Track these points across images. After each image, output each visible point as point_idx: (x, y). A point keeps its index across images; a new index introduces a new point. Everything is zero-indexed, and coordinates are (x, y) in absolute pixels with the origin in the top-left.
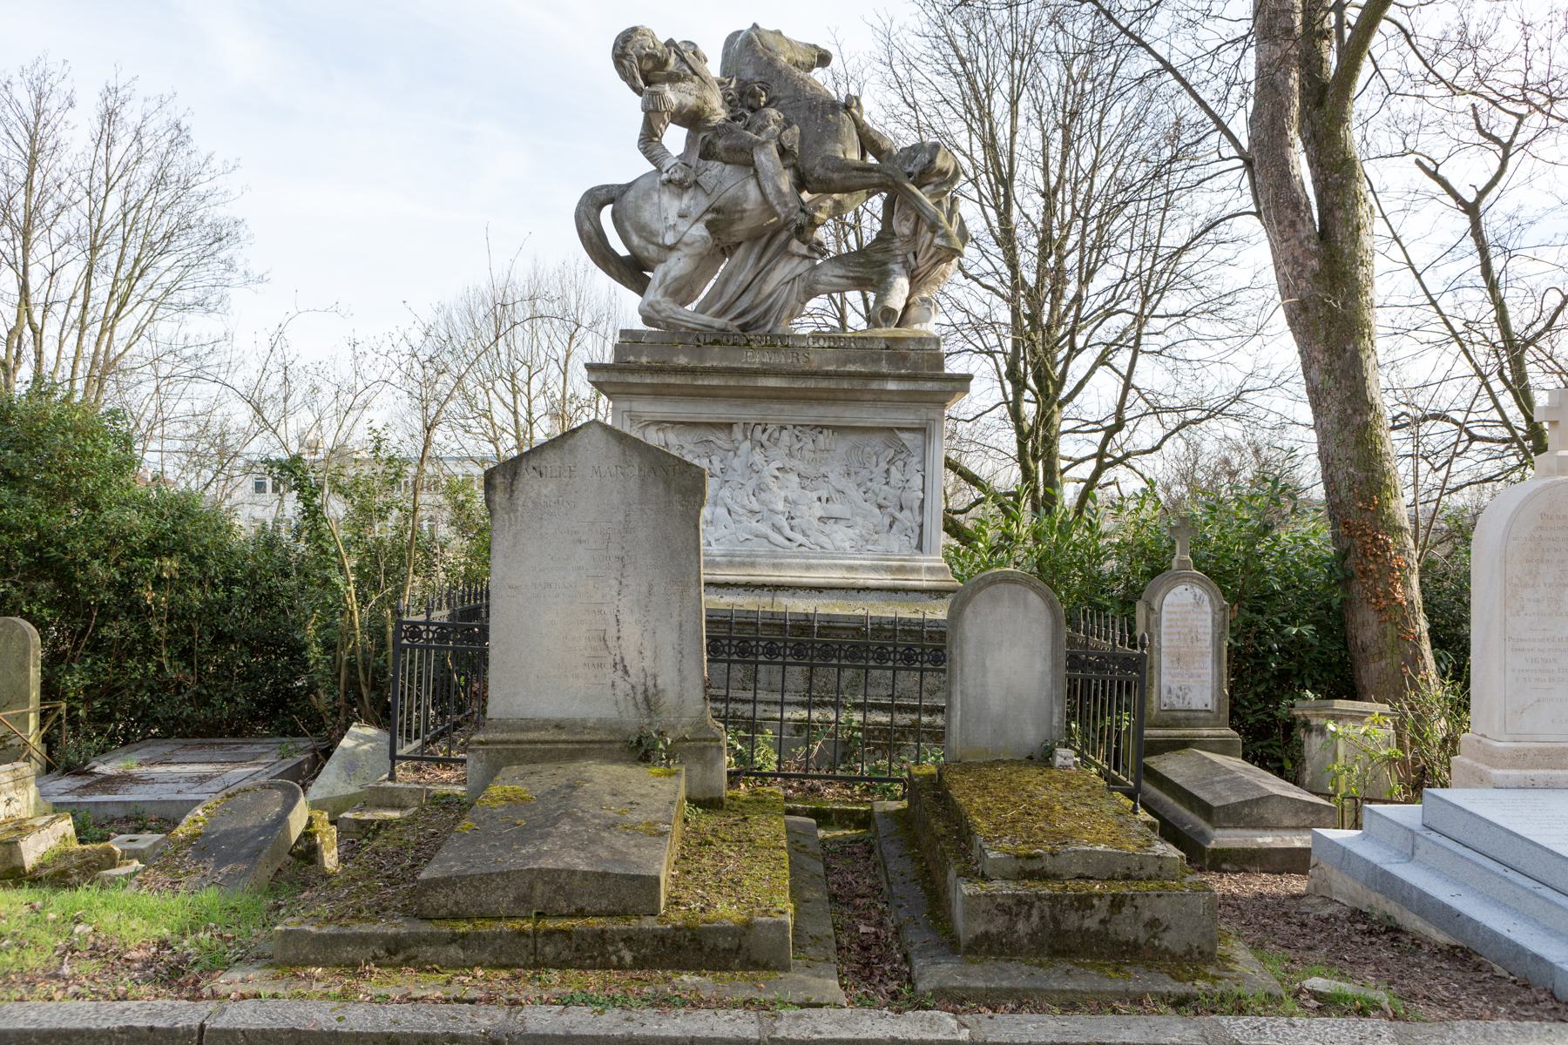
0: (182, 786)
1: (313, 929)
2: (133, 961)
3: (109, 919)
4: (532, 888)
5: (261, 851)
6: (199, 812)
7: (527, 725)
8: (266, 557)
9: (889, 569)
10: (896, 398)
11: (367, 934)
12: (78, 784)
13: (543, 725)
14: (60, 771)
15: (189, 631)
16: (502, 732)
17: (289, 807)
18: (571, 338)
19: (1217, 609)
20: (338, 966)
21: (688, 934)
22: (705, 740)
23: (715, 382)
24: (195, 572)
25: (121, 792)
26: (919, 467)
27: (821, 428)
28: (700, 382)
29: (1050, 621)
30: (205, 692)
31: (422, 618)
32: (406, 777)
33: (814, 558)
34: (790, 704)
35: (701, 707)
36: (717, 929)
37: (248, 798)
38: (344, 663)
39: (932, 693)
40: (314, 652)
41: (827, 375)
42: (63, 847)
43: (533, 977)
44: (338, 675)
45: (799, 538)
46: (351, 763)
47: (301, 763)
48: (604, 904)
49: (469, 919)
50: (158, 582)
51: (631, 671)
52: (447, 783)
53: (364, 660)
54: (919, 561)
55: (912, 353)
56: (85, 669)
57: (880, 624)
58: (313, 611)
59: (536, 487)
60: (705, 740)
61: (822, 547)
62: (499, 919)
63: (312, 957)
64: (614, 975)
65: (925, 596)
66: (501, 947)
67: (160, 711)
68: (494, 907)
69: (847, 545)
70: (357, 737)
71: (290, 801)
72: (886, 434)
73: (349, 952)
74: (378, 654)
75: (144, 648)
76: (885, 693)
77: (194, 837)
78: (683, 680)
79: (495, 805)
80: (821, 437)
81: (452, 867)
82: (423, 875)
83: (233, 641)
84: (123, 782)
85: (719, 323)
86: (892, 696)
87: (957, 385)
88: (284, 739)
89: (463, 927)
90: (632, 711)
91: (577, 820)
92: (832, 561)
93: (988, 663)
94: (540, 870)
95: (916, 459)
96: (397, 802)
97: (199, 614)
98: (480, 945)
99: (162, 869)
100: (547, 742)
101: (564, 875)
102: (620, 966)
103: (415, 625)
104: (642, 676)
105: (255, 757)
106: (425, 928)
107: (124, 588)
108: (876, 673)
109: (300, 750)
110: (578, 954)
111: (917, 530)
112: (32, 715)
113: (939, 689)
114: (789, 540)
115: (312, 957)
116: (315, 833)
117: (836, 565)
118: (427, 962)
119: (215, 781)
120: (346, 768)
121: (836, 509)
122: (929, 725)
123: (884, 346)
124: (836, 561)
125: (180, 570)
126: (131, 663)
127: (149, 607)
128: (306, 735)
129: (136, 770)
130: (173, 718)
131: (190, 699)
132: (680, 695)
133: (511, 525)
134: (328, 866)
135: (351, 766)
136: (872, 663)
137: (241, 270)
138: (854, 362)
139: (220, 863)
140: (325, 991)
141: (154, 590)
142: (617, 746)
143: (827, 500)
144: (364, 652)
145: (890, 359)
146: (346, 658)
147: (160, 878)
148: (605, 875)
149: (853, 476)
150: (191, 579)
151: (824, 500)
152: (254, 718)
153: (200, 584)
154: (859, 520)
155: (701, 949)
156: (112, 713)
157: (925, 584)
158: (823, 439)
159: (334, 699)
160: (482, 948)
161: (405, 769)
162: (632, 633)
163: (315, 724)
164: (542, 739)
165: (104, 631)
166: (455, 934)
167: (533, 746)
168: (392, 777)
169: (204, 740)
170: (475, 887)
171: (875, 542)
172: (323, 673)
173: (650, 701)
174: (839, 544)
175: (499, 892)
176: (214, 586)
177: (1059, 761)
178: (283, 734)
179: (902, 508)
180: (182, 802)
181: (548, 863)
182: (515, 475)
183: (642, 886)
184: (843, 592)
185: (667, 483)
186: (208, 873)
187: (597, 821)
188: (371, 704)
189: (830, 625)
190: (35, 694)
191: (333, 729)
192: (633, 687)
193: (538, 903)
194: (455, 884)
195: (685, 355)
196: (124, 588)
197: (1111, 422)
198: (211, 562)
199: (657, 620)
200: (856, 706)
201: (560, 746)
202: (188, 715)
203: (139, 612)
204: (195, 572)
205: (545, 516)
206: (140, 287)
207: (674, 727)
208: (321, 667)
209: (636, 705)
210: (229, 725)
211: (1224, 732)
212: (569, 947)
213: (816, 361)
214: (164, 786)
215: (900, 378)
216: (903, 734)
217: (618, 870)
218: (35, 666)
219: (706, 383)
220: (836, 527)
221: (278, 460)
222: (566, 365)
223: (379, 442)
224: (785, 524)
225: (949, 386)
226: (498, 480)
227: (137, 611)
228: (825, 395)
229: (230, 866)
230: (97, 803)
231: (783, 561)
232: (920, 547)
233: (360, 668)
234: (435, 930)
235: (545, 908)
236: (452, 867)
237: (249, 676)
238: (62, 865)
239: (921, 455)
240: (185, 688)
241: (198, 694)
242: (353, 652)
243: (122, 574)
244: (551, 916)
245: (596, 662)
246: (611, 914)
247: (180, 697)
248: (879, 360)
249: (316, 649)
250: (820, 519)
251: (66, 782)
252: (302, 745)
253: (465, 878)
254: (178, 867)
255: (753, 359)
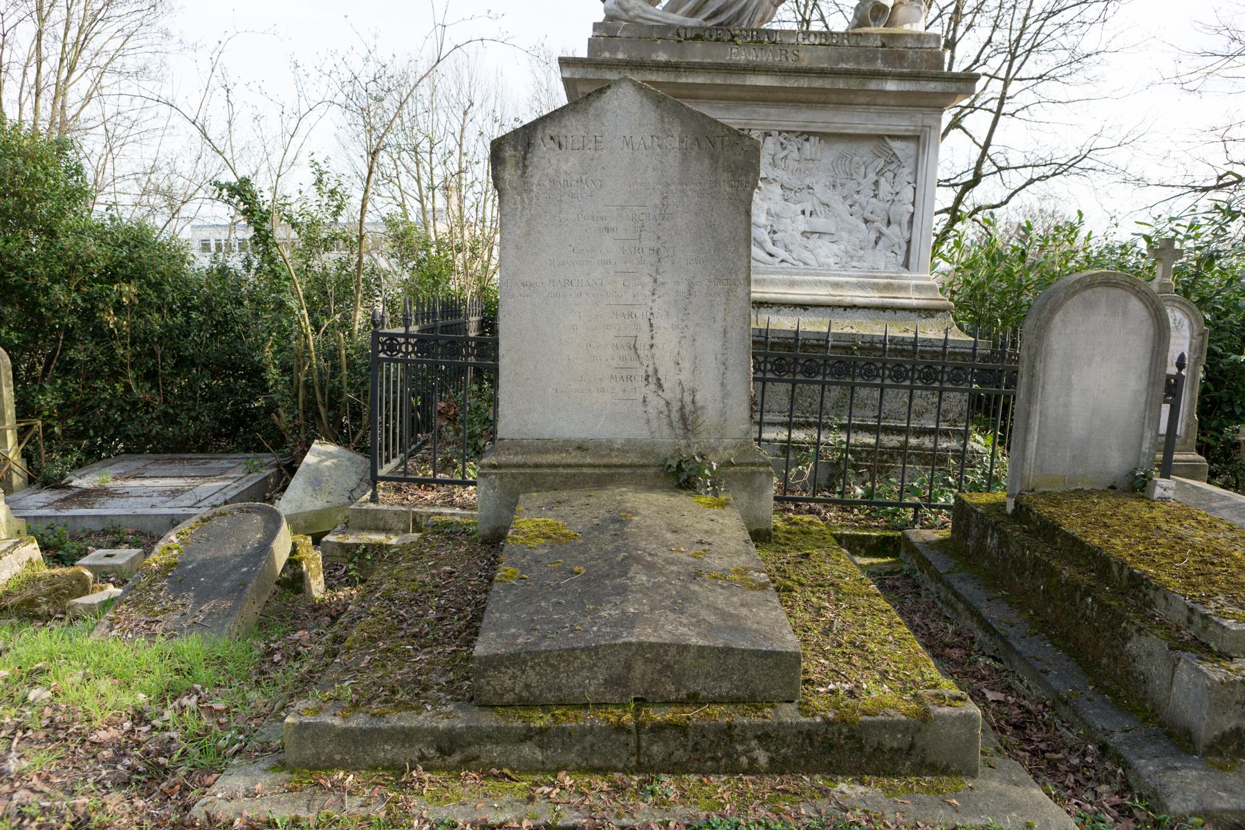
0: (156, 500)
1: (337, 722)
2: (100, 745)
3: (69, 678)
4: (629, 667)
5: (245, 585)
6: (173, 538)
7: (545, 446)
8: (220, 286)
9: (876, 287)
10: (892, 102)
11: (411, 729)
12: (56, 497)
13: (564, 446)
14: (38, 485)
15: (152, 354)
16: (516, 454)
17: (271, 534)
18: (465, 113)
19: (1195, 334)
20: (375, 768)
21: (845, 730)
22: (753, 464)
23: (700, 79)
24: (153, 297)
25: (97, 506)
26: (910, 179)
27: (807, 135)
28: (683, 80)
29: (1151, 331)
30: (171, 411)
31: (401, 330)
32: (388, 501)
33: (798, 274)
34: (769, 424)
35: (745, 427)
36: (883, 724)
37: (225, 523)
38: (301, 384)
39: (920, 415)
40: (273, 373)
41: (822, 73)
42: (30, 572)
43: (641, 784)
44: (296, 395)
45: (782, 253)
46: (316, 478)
47: (266, 478)
48: (725, 688)
49: (545, 707)
50: (119, 308)
51: (665, 386)
52: (432, 504)
53: (321, 381)
54: (906, 278)
55: (911, 52)
56: (56, 390)
57: (872, 343)
58: (270, 334)
59: (554, 161)
60: (753, 464)
61: (805, 263)
62: (585, 706)
63: (338, 757)
64: (749, 784)
65: (914, 315)
66: (592, 745)
67: (131, 428)
68: (577, 691)
69: (832, 261)
70: (319, 453)
71: (272, 526)
72: (874, 143)
73: (387, 752)
74: (333, 376)
75: (111, 370)
76: (871, 414)
77: (168, 567)
78: (726, 395)
79: (532, 544)
80: (807, 145)
81: (515, 636)
82: (480, 649)
83: (194, 365)
84: (99, 496)
85: (691, 22)
86: (878, 417)
87: (961, 85)
88: (248, 455)
89: (541, 720)
90: (666, 431)
91: (650, 567)
92: (817, 278)
93: (1074, 379)
94: (640, 644)
95: (907, 170)
96: (381, 525)
97: (160, 338)
98: (563, 743)
99: (136, 605)
100: (569, 466)
101: (673, 651)
102: (752, 769)
103: (392, 337)
104: (678, 390)
105: (222, 472)
106: (489, 720)
107: (88, 314)
108: (863, 393)
109: (265, 466)
110: (697, 755)
111: (904, 247)
112: (9, 432)
113: (927, 410)
114: (771, 255)
115: (338, 757)
116: (301, 560)
117: (820, 282)
118: (492, 764)
119: (187, 495)
120: (311, 483)
121: (820, 223)
122: (918, 447)
123: (879, 44)
124: (821, 278)
125: (139, 295)
126: (99, 384)
127: (112, 331)
128: (269, 451)
129: (111, 484)
130: (144, 435)
131: (158, 418)
132: (723, 413)
133: (524, 208)
134: (316, 594)
135: (316, 482)
136: (888, 382)
137: (176, 39)
138: (847, 61)
139: (202, 597)
140: (363, 812)
141: (115, 315)
142: (652, 471)
143: (811, 214)
144: (320, 374)
145: (886, 60)
146: (303, 379)
147: (134, 616)
148: (728, 651)
149: (839, 188)
150: (150, 305)
151: (808, 213)
152: (218, 435)
153: (159, 310)
154: (844, 234)
155: (861, 748)
156: (86, 430)
157: (914, 303)
158: (810, 148)
159: (294, 418)
160: (566, 748)
161: (384, 489)
162: (668, 340)
163: (277, 440)
164: (564, 462)
165: (71, 353)
166: (530, 729)
167: (554, 471)
168: (374, 499)
169: (174, 456)
170: (552, 666)
171: (861, 259)
172: (283, 394)
173: (687, 420)
174: (823, 260)
175: (585, 673)
176: (172, 312)
177: (1158, 492)
178: (247, 450)
179: (889, 223)
180: (156, 516)
181: (645, 634)
182: (528, 146)
183: (777, 666)
184: (829, 310)
185: (714, 158)
186: (188, 611)
187: (674, 568)
188: (329, 422)
189: (821, 342)
190: (10, 412)
191: (295, 446)
192: (668, 404)
193: (638, 685)
194: (525, 662)
195: (665, 52)
196: (88, 314)
197: (969, 177)
198: (168, 288)
199: (697, 325)
200: (842, 427)
201: (585, 470)
202: (157, 433)
203: (103, 336)
204: (153, 297)
205: (565, 198)
206: (85, 53)
207: (714, 450)
208: (280, 387)
209: (671, 424)
210: (196, 442)
211: (1191, 457)
212: (684, 747)
213: (806, 60)
214: (139, 500)
215: (901, 77)
216: (891, 456)
217: (744, 645)
218: (8, 385)
219: (690, 80)
220: (820, 242)
221: (229, 184)
222: (461, 138)
223: (321, 174)
224: (767, 238)
225: (953, 87)
226: (508, 152)
227: (101, 335)
228: (815, 97)
229: (212, 603)
230: (74, 517)
231: (765, 277)
232: (906, 265)
233: (317, 389)
234: (503, 724)
235: (646, 693)
236: (515, 636)
237: (213, 396)
238: (29, 593)
239: (913, 166)
240: (153, 408)
241: (166, 414)
242: (309, 373)
243: (84, 300)
244: (654, 703)
245: (625, 373)
246: (734, 701)
247: (149, 416)
248: (875, 59)
249: (274, 371)
250: (803, 233)
251: (45, 496)
252: (266, 461)
253: (538, 654)
254: (153, 603)
255: (739, 55)
